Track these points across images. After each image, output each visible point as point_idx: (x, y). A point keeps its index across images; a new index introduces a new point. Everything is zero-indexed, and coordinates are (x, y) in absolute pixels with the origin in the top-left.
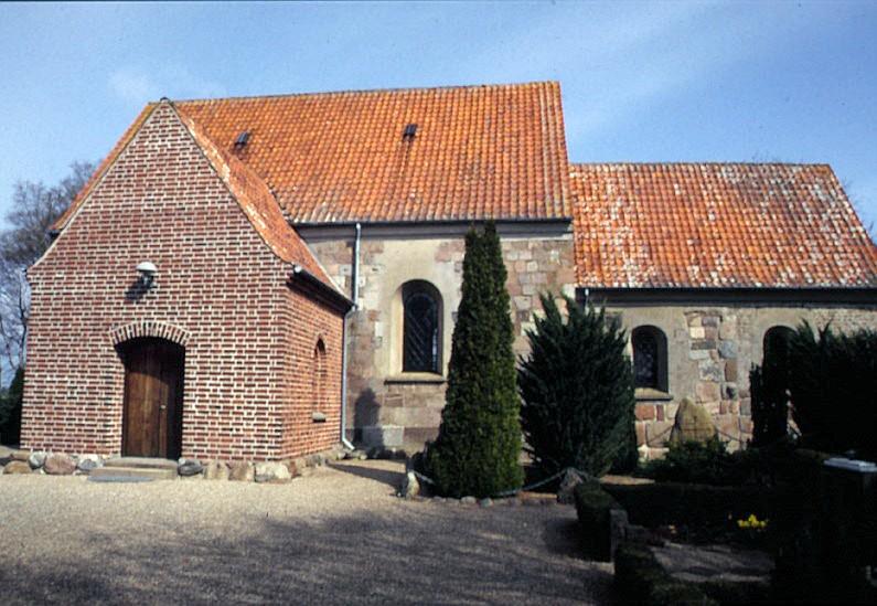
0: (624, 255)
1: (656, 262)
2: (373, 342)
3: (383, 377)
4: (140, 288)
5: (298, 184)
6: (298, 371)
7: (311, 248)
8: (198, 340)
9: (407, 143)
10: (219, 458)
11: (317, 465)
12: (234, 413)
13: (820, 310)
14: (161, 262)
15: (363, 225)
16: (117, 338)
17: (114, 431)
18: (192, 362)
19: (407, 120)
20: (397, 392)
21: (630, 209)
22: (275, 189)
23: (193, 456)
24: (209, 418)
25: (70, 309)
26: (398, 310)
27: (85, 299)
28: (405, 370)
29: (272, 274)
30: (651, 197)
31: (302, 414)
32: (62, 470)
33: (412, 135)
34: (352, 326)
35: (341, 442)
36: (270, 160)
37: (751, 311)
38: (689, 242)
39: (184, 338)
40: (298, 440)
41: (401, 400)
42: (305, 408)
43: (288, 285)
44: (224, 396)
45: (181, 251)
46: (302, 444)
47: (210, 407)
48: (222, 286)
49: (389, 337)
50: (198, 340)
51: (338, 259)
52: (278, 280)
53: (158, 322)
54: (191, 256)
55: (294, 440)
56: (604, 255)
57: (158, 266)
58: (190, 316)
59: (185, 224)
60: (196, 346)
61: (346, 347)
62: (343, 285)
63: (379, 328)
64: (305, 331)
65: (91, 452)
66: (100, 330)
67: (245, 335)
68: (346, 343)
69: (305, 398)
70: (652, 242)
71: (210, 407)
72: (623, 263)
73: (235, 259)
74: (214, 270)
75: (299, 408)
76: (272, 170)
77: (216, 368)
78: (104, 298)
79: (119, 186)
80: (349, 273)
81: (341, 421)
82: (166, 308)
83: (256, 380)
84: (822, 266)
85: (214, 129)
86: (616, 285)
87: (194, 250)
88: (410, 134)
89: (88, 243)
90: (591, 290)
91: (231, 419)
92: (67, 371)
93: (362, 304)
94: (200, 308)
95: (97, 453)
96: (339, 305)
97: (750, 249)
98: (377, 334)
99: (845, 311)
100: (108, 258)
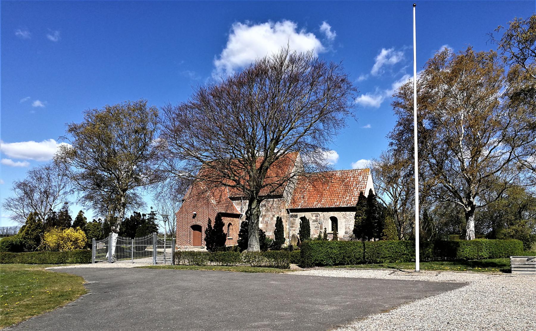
99: (349, 212)
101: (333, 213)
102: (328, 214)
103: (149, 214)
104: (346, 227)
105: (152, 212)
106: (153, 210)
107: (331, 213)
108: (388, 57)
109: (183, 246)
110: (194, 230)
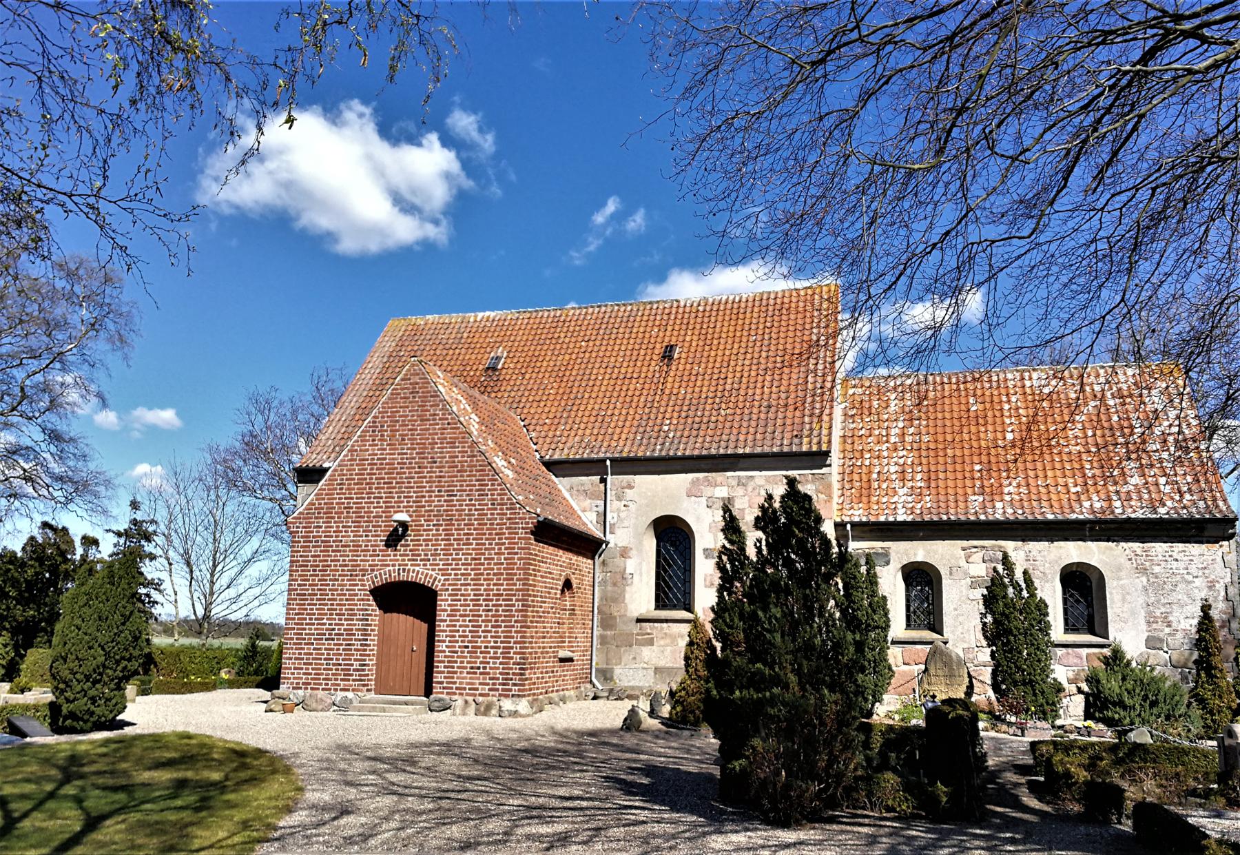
0: (897, 484)
1: (933, 491)
2: (624, 578)
3: (636, 615)
4: (395, 538)
5: (551, 416)
6: (544, 612)
7: (563, 485)
8: (449, 585)
9: (665, 368)
10: (467, 694)
11: (561, 703)
12: (481, 653)
13: (1131, 544)
14: (414, 512)
15: (612, 460)
16: (373, 582)
17: (369, 670)
18: (444, 605)
19: (667, 339)
20: (649, 631)
21: (911, 430)
22: (527, 422)
23: (442, 693)
24: (458, 657)
25: (329, 556)
26: (650, 544)
27: (342, 546)
28: (657, 608)
29: (517, 523)
30: (940, 415)
31: (547, 653)
32: (320, 707)
33: (671, 358)
34: (604, 563)
35: (591, 682)
36: (522, 388)
37: (1044, 545)
38: (977, 467)
39: (436, 583)
40: (543, 678)
41: (653, 638)
42: (550, 647)
43: (532, 533)
44: (509, 533)
45: (434, 501)
46: (546, 682)
47: (460, 647)
48: (472, 534)
49: (641, 574)
50: (449, 585)
51: (593, 496)
52: (523, 528)
53: (412, 568)
54: (443, 506)
55: (538, 678)
56: (875, 485)
57: (411, 516)
58: (441, 563)
59: (436, 477)
60: (447, 590)
61: (596, 585)
62: (594, 522)
63: (631, 565)
64: (550, 573)
65: (348, 690)
66: (356, 575)
67: (492, 580)
68: (597, 581)
69: (551, 637)
70: (933, 468)
71: (460, 647)
72: (896, 493)
73: (483, 510)
74: (464, 520)
75: (544, 648)
76: (524, 400)
77: (466, 610)
78: (361, 546)
79: (373, 440)
80: (601, 509)
81: (591, 660)
82: (420, 555)
83: (503, 621)
84: (1139, 492)
85: (463, 351)
86: (882, 519)
87: (445, 501)
88: (668, 354)
89: (345, 494)
90: (854, 525)
91: (478, 658)
92: (326, 614)
93: (615, 540)
94: (451, 554)
95: (353, 690)
96: (587, 545)
97: (1050, 473)
98: (628, 571)
99: (1165, 546)
100: (364, 508)
101: (1098, 547)
102: (235, 695)
103: (119, 534)
104: (1150, 614)
105: (135, 522)
106: (139, 516)
107: (1071, 545)
108: (620, 217)
109: (320, 694)
110: (385, 612)
